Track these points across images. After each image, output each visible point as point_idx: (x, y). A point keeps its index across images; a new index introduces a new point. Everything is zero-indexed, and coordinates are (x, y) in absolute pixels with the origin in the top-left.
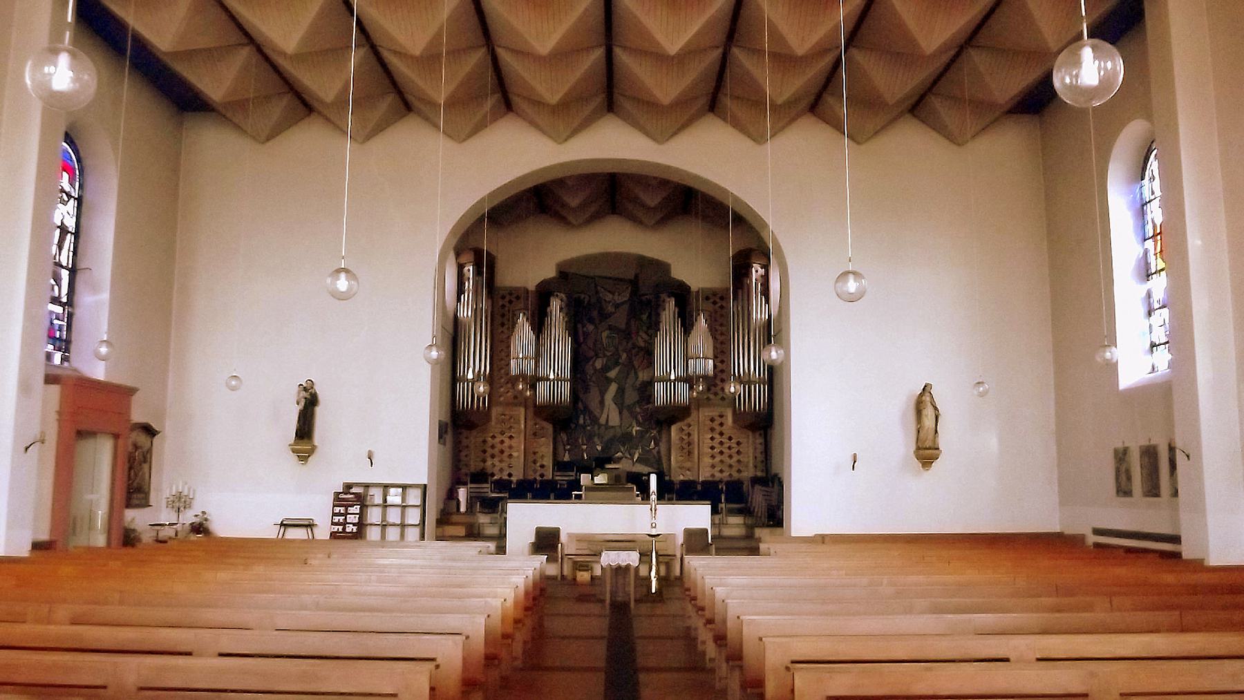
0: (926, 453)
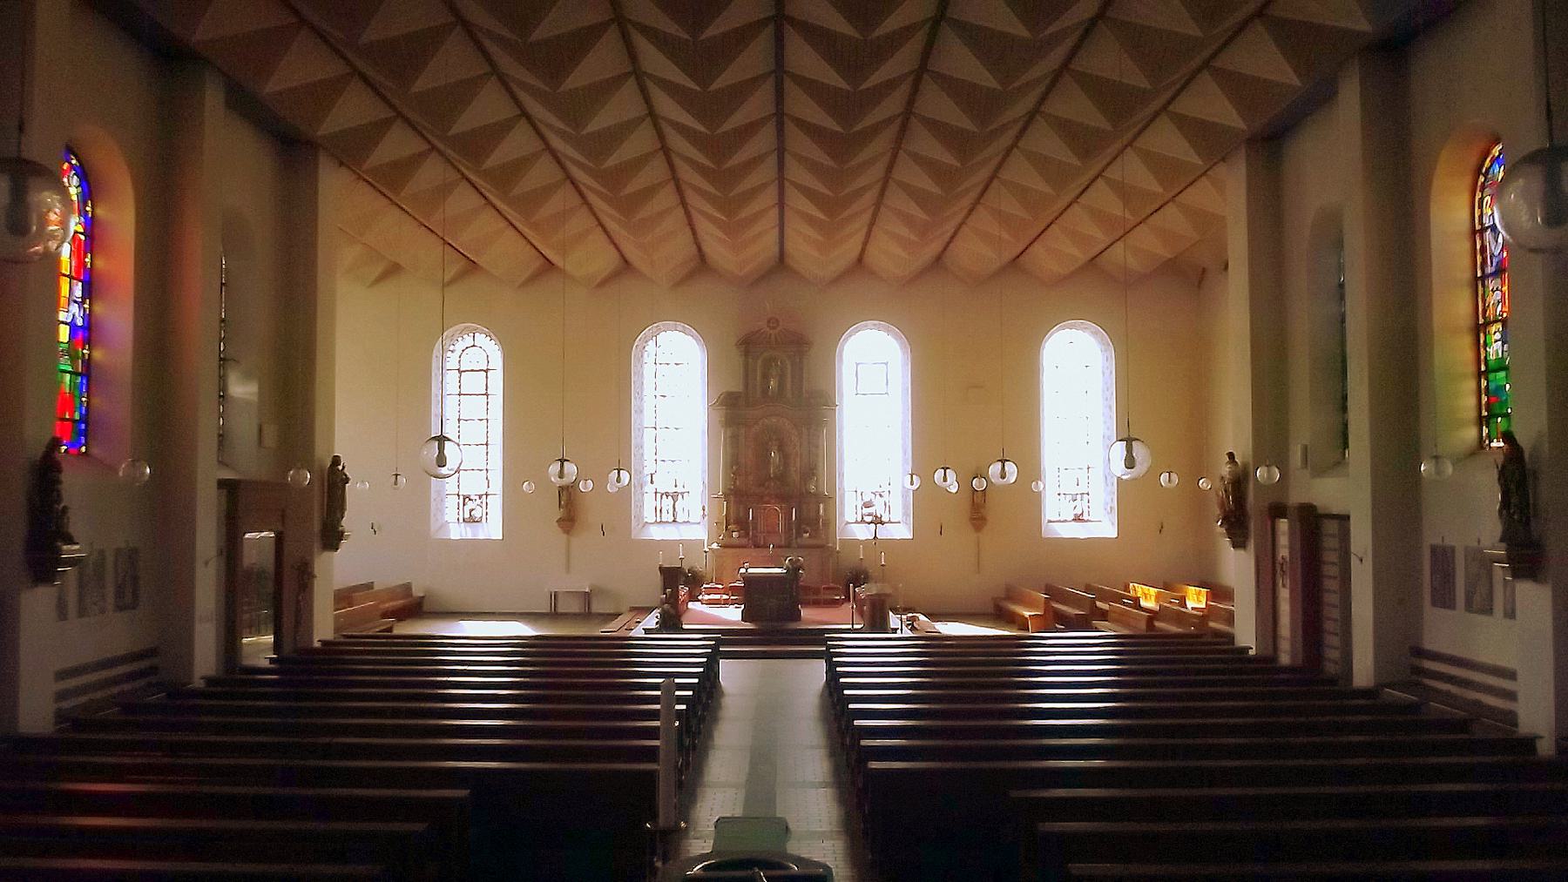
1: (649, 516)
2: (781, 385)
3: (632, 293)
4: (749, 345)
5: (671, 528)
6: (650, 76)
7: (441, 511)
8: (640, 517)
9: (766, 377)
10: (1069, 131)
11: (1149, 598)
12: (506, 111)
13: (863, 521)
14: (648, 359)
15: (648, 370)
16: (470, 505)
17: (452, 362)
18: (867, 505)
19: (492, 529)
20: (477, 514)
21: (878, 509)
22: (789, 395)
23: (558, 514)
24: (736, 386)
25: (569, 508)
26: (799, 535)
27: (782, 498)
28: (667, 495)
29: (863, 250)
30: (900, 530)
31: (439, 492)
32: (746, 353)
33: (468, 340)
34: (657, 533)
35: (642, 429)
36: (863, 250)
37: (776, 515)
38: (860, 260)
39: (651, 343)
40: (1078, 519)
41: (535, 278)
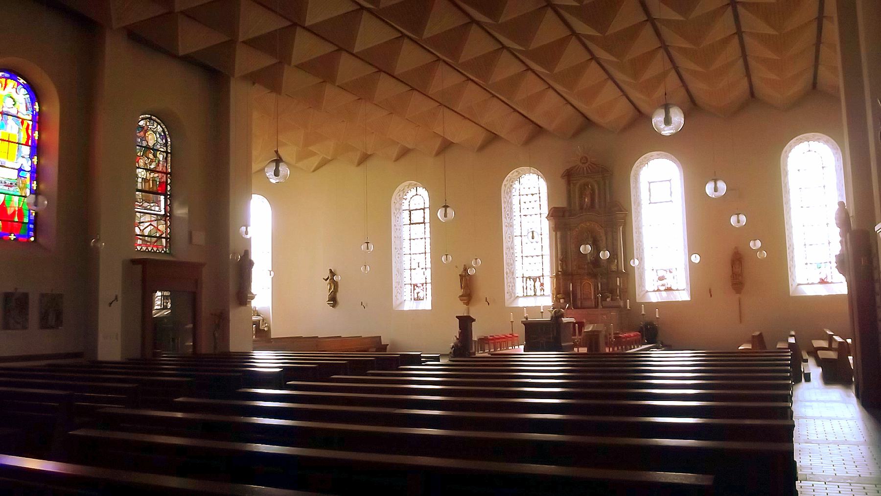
1: (519, 291)
2: (592, 200)
3: (497, 150)
4: (569, 176)
5: (533, 299)
6: (557, 5)
7: (401, 293)
8: (512, 292)
9: (581, 196)
10: (254, 78)
11: (838, 339)
12: (561, 32)
13: (658, 290)
14: (515, 193)
15: (515, 201)
16: (417, 290)
17: (405, 206)
18: (661, 279)
19: (426, 305)
20: (421, 295)
21: (669, 282)
22: (597, 206)
23: (461, 292)
24: (562, 203)
25: (468, 288)
26: (604, 299)
27: (594, 276)
28: (530, 278)
29: (688, 91)
30: (684, 296)
31: (398, 283)
32: (569, 183)
33: (413, 192)
34: (522, 303)
35: (512, 237)
36: (688, 91)
37: (589, 288)
38: (814, 85)
39: (517, 183)
40: (823, 282)
41: (482, 148)
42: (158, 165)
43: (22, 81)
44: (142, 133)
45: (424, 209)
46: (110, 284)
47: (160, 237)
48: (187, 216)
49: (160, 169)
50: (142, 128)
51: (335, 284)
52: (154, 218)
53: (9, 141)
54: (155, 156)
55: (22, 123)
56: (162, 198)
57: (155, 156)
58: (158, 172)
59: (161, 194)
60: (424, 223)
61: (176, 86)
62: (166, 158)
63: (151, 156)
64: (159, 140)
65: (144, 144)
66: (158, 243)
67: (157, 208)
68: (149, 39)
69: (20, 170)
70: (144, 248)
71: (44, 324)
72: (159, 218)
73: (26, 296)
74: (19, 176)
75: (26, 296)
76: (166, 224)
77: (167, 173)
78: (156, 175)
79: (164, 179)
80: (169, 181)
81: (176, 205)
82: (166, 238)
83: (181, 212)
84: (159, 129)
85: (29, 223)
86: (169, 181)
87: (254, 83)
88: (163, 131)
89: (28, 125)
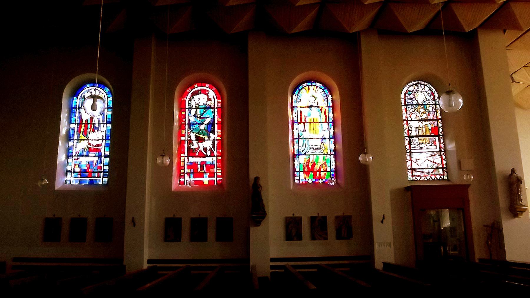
0: (133, 220)
42: (429, 115)
43: (318, 84)
44: (412, 96)
45: (78, 140)
46: (382, 206)
47: (437, 168)
48: (455, 149)
49: (430, 117)
50: (412, 92)
51: (384, 218)
52: (428, 154)
53: (314, 123)
54: (425, 109)
55: (321, 110)
56: (437, 138)
57: (425, 109)
58: (429, 120)
59: (435, 136)
60: (410, 137)
61: (439, 54)
62: (435, 109)
63: (422, 110)
64: (428, 97)
65: (415, 102)
66: (436, 173)
67: (433, 147)
68: (387, 28)
69: (322, 139)
70: (423, 178)
71: (339, 236)
72: (434, 153)
73: (325, 218)
74: (322, 143)
75: (325, 218)
76: (441, 157)
77: (437, 120)
78: (428, 122)
79: (436, 124)
80: (440, 125)
81: (447, 142)
82: (443, 168)
83: (451, 146)
84: (427, 89)
85: (331, 171)
86: (440, 125)
87: (505, 32)
88: (430, 90)
89: (326, 110)
